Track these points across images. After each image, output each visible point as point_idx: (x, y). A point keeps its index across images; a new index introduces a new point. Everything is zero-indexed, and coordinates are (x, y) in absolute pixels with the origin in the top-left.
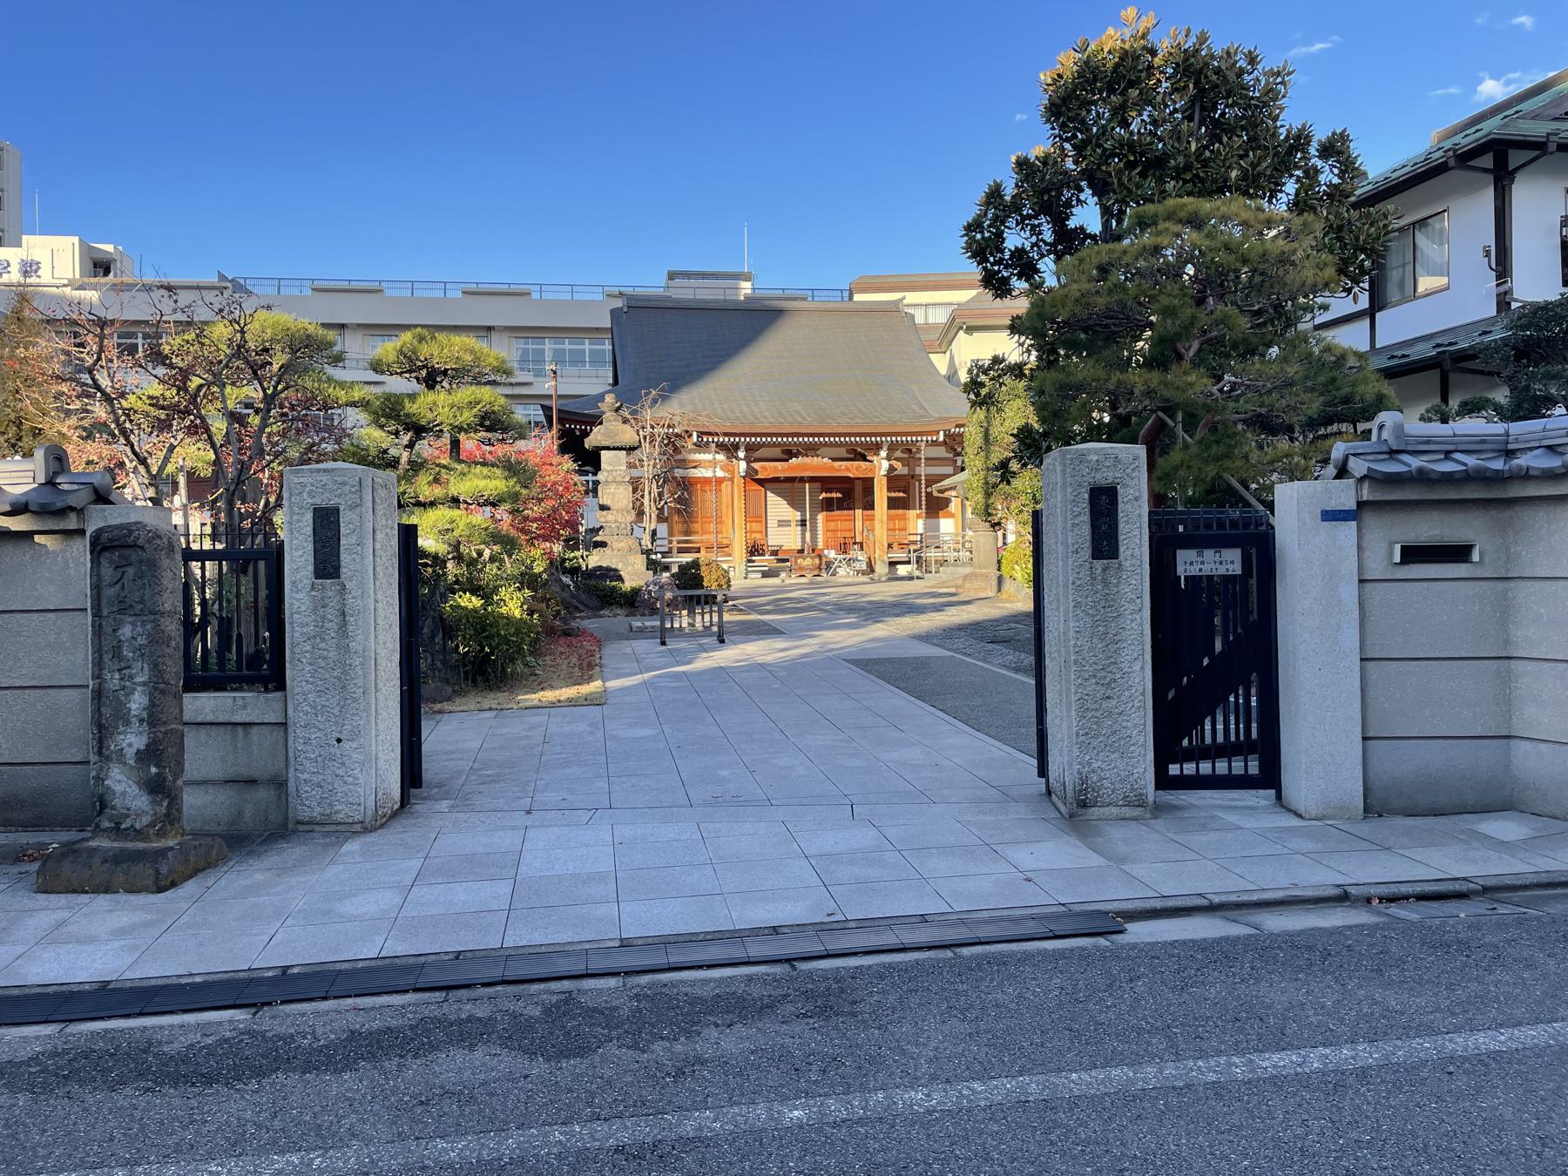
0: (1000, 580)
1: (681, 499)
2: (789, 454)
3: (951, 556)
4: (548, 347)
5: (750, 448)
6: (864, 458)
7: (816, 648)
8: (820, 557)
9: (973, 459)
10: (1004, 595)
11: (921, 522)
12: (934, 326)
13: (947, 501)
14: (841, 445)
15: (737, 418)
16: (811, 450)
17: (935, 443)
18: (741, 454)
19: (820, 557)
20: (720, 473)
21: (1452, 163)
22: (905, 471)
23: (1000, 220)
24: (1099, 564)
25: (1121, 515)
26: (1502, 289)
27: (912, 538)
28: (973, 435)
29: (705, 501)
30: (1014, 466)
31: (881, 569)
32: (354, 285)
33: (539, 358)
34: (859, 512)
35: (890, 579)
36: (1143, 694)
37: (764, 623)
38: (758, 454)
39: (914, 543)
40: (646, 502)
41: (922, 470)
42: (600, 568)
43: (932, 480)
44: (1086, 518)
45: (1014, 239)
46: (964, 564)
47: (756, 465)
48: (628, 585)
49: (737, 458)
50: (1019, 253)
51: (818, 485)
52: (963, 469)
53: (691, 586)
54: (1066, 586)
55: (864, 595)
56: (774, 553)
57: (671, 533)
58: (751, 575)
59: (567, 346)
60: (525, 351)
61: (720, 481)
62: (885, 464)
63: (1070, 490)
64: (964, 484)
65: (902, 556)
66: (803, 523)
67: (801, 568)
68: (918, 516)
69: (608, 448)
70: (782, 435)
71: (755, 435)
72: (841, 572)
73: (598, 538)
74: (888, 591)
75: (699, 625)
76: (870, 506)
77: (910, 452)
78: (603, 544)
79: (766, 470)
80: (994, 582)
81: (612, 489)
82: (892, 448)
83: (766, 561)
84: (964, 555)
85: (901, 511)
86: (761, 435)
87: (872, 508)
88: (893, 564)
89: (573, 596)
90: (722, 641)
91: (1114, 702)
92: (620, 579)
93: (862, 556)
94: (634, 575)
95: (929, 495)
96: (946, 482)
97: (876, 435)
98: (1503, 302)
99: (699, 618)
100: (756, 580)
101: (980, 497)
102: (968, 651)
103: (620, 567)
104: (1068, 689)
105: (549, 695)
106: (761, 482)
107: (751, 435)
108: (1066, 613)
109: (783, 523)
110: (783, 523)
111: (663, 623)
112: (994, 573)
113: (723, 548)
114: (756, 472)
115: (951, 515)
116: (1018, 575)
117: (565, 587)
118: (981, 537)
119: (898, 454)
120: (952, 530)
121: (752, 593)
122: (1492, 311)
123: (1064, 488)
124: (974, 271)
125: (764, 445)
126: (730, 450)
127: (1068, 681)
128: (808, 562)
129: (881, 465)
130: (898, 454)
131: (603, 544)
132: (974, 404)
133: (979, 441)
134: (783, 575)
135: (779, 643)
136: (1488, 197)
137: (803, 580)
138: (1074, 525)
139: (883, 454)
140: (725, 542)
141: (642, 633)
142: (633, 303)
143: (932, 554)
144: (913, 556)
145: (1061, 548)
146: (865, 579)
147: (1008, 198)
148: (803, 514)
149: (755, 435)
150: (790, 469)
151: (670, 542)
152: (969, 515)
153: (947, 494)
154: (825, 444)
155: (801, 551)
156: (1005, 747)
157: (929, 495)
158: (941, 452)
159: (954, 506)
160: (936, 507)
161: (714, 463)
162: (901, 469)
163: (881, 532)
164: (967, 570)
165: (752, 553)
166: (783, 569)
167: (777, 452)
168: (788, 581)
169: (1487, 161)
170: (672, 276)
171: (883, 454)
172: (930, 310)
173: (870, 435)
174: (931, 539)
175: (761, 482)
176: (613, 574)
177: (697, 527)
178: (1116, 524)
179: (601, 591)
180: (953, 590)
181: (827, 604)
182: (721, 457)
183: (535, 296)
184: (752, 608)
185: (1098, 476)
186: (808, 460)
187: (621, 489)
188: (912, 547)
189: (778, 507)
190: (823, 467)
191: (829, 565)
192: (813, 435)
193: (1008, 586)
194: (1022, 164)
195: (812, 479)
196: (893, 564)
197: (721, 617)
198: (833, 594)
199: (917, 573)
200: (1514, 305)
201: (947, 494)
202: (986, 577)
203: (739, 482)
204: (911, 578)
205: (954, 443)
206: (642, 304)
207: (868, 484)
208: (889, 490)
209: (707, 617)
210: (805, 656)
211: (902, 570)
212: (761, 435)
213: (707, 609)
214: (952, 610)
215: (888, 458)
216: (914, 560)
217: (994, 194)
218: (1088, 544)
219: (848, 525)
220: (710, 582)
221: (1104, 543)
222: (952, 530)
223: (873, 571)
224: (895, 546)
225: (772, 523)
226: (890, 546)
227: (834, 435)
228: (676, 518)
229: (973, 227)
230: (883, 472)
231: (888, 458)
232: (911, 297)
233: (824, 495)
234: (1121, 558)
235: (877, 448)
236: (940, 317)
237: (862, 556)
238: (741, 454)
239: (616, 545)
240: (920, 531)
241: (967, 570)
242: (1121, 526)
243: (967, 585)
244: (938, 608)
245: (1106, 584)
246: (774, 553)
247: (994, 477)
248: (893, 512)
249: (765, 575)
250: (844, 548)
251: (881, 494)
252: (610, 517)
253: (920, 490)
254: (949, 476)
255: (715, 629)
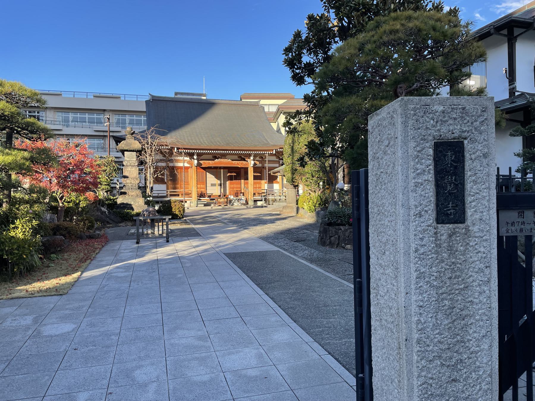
0: (298, 209)
1: (170, 175)
2: (215, 157)
3: (278, 198)
4: (128, 118)
5: (199, 155)
6: (244, 160)
7: (213, 245)
8: (227, 198)
9: (287, 159)
10: (299, 215)
11: (266, 185)
12: (272, 113)
13: (276, 177)
14: (235, 154)
15: (194, 143)
16: (223, 156)
17: (272, 155)
18: (195, 157)
19: (227, 198)
20: (186, 165)
21: (492, 31)
22: (260, 165)
23: (300, 48)
24: (445, 229)
25: (468, 173)
26: (512, 87)
27: (263, 191)
28: (287, 150)
29: (180, 176)
30: (307, 159)
31: (251, 203)
32: (50, 92)
33: (124, 122)
34: (243, 181)
35: (254, 207)
36: (490, 376)
37: (194, 229)
38: (202, 157)
39: (264, 193)
40: (148, 175)
41: (267, 165)
42: (123, 204)
43: (270, 169)
44: (430, 176)
45: (306, 58)
46: (283, 202)
47: (201, 162)
48: (136, 211)
49: (193, 159)
50: (308, 65)
51: (227, 170)
52: (282, 165)
53: (166, 210)
54: (407, 254)
55: (242, 215)
56: (209, 197)
57: (168, 189)
58: (199, 205)
59: (135, 118)
60: (119, 119)
61: (187, 168)
62: (253, 162)
63: (412, 144)
64: (283, 171)
65: (258, 198)
66: (221, 185)
67: (220, 203)
68: (265, 183)
69: (127, 151)
70: (211, 150)
71: (201, 149)
72: (235, 204)
73: (123, 191)
74: (252, 213)
75: (156, 233)
76: (247, 179)
77: (262, 158)
78: (125, 193)
79: (205, 163)
80: (295, 210)
81: (129, 169)
82: (255, 156)
83: (206, 200)
84: (283, 198)
85: (259, 181)
86: (203, 150)
87: (248, 179)
88: (255, 201)
89: (107, 217)
90: (168, 241)
91: (460, 386)
92: (133, 209)
93: (243, 198)
94: (138, 205)
95: (269, 174)
96: (276, 170)
97: (249, 150)
98: (512, 92)
99: (156, 229)
100: (201, 207)
101: (290, 175)
102: (286, 247)
103: (132, 203)
104: (410, 372)
105: (37, 286)
106: (204, 169)
107: (199, 149)
108: (408, 286)
109: (213, 185)
110: (213, 185)
111: (138, 230)
112: (294, 205)
113: (188, 194)
114: (201, 164)
115: (278, 183)
116: (306, 207)
117: (103, 213)
118: (290, 191)
119: (258, 158)
120: (278, 188)
121: (197, 213)
122: (507, 96)
123: (405, 143)
124: (288, 73)
125: (204, 154)
126: (191, 155)
127: (409, 362)
128: (222, 200)
129: (251, 162)
130: (258, 158)
131: (125, 193)
132: (288, 132)
133: (289, 151)
134: (212, 205)
135: (195, 242)
136: (504, 50)
137: (220, 207)
138: (417, 185)
139: (252, 158)
140: (190, 192)
141: (128, 237)
142: (155, 98)
143: (270, 197)
144: (263, 198)
145: (401, 211)
146: (244, 207)
147: (303, 38)
148: (221, 182)
149: (201, 149)
150: (215, 163)
151: (167, 192)
152: (285, 182)
153: (276, 174)
154: (229, 154)
155: (220, 196)
156: (316, 345)
157: (269, 174)
158: (274, 158)
159: (279, 179)
160: (272, 179)
161: (184, 161)
162: (259, 165)
163: (251, 189)
164: (284, 204)
165: (200, 197)
166: (213, 203)
167: (210, 157)
168: (214, 208)
169: (505, 32)
170: (176, 94)
171: (252, 158)
172: (270, 107)
173: (247, 150)
174: (271, 191)
175: (204, 169)
176: (129, 207)
177: (178, 186)
178: (463, 184)
179: (121, 214)
180: (278, 213)
181: (226, 219)
182: (187, 159)
183: (122, 99)
184: (193, 222)
185: (444, 129)
186: (222, 160)
187: (134, 169)
188: (263, 195)
189: (211, 178)
190: (229, 163)
191: (230, 201)
192: (224, 150)
193: (301, 211)
194: (311, 18)
195: (224, 168)
196: (255, 201)
197: (167, 227)
198: (230, 214)
199: (265, 205)
200: (517, 94)
201: (276, 174)
202: (291, 207)
203: (194, 168)
204: (262, 207)
205: (279, 155)
206: (157, 99)
207: (246, 169)
208: (254, 172)
209: (161, 229)
210: (206, 251)
211: (259, 203)
212: (203, 150)
213: (160, 224)
214: (278, 222)
215: (254, 160)
216: (263, 199)
217: (298, 35)
218: (432, 206)
219: (239, 186)
220: (176, 210)
221: (450, 206)
222: (278, 188)
223: (248, 204)
224: (257, 194)
225: (209, 184)
226: (254, 194)
227: (232, 150)
228: (170, 182)
229: (288, 50)
230: (252, 165)
231: (254, 160)
232: (262, 102)
233: (229, 174)
234: (469, 222)
235: (249, 156)
236: (274, 109)
237: (243, 198)
238: (195, 157)
239: (130, 193)
240: (266, 188)
241: (284, 204)
242: (469, 185)
243: (284, 211)
244: (272, 221)
245: (451, 250)
246: (209, 197)
247: (297, 166)
248: (256, 181)
249: (205, 205)
250: (237, 195)
251: (251, 174)
252: (128, 181)
253: (266, 173)
254: (277, 167)
255: (165, 235)
